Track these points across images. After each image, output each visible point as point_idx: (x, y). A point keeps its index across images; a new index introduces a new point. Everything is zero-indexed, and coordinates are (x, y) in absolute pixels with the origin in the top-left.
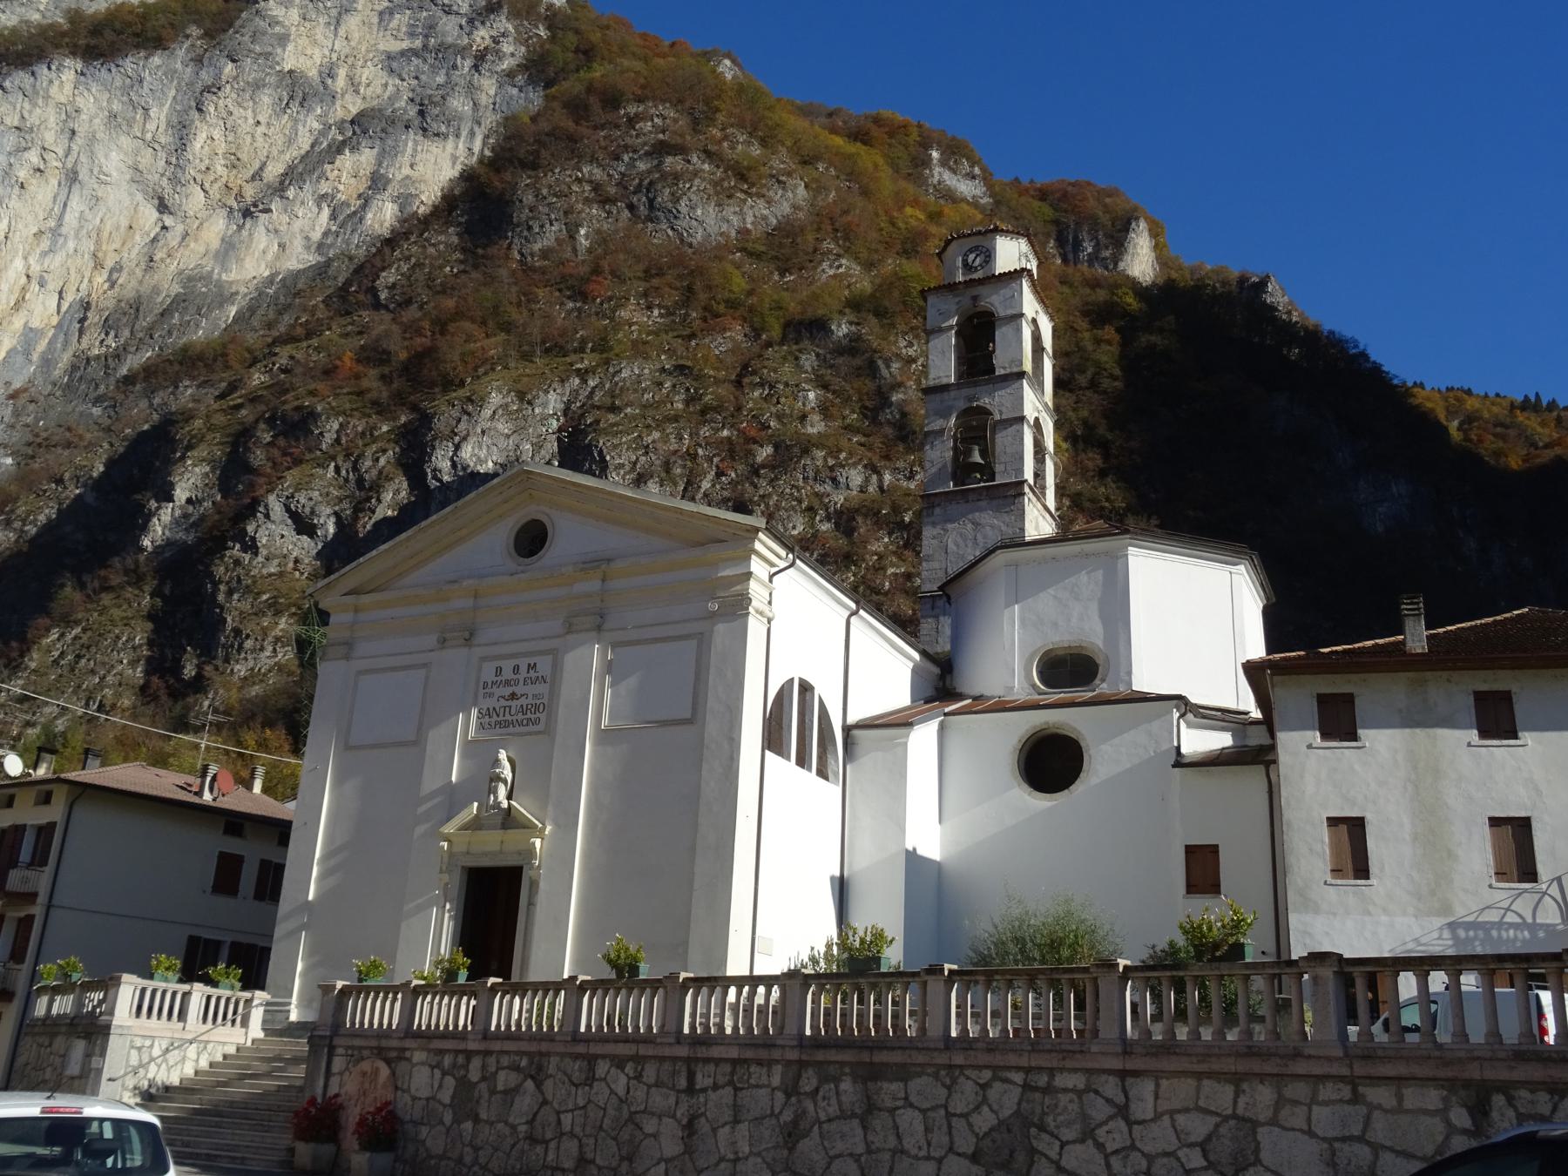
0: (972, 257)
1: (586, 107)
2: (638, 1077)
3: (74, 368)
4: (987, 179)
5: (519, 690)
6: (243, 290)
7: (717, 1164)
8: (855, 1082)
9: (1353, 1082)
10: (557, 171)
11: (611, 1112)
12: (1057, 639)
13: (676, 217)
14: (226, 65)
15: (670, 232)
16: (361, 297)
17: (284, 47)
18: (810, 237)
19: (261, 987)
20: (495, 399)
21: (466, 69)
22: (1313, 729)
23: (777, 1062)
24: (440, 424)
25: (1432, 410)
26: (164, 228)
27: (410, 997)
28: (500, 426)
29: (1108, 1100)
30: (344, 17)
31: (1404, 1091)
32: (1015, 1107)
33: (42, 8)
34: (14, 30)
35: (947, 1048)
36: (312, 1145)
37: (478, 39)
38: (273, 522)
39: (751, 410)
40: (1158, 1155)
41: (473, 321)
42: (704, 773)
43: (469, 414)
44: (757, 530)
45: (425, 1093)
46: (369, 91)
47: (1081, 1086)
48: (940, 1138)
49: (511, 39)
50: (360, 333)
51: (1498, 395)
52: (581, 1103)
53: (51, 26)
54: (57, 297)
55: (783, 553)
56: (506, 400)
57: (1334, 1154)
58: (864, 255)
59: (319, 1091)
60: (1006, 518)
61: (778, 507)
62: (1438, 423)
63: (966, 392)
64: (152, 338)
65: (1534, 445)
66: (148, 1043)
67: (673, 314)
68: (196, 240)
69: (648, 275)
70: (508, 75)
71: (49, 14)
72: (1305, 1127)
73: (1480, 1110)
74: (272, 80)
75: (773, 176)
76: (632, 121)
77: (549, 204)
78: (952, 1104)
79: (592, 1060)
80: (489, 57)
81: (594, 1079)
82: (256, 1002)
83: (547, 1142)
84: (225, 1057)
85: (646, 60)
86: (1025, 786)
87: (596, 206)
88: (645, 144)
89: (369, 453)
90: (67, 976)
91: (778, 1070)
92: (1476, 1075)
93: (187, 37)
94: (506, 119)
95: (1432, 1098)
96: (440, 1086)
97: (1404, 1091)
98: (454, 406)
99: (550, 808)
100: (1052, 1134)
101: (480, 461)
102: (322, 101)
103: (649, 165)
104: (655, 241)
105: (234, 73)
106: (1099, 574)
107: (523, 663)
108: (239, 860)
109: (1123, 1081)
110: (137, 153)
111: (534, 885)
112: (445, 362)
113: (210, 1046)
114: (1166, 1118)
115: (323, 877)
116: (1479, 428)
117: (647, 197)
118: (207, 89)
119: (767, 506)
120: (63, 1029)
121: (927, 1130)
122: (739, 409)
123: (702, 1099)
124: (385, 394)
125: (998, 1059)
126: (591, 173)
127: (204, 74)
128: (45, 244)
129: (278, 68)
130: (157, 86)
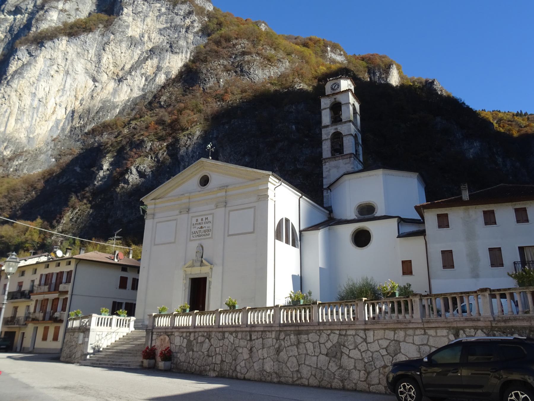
2: (236, 337)
3: (71, 131)
4: (345, 55)
5: (203, 225)
6: (120, 104)
7: (259, 360)
8: (294, 335)
9: (424, 329)
11: (229, 347)
13: (249, 74)
14: (111, 36)
15: (248, 79)
17: (128, 29)
18: (291, 78)
19: (134, 315)
21: (184, 32)
23: (274, 331)
25: (488, 118)
26: (96, 86)
27: (194, 316)
29: (361, 337)
30: (146, 18)
31: (437, 331)
32: (337, 340)
33: (55, 22)
34: (47, 29)
35: (319, 325)
36: (148, 360)
38: (133, 175)
40: (375, 352)
41: (190, 109)
43: (190, 139)
44: (270, 175)
45: (178, 344)
46: (155, 41)
47: (354, 334)
48: (317, 350)
49: (197, 22)
51: (509, 112)
52: (221, 345)
53: (58, 27)
54: (65, 109)
55: (277, 181)
57: (420, 349)
58: (308, 82)
59: (149, 345)
62: (490, 122)
64: (94, 120)
65: (521, 127)
66: (101, 333)
68: (105, 89)
71: (57, 24)
72: (412, 342)
73: (457, 335)
74: (125, 39)
76: (234, 45)
77: (211, 73)
78: (320, 340)
79: (224, 333)
80: (190, 28)
81: (224, 338)
82: (131, 320)
83: (212, 356)
84: (123, 336)
85: (238, 26)
88: (239, 52)
90: (77, 315)
91: (274, 333)
92: (455, 326)
93: (99, 28)
94: (196, 47)
95: (445, 332)
96: (183, 342)
97: (437, 331)
100: (347, 348)
102: (141, 45)
105: (114, 38)
107: (204, 218)
108: (126, 278)
109: (365, 332)
110: (86, 64)
111: (210, 282)
113: (119, 333)
114: (376, 341)
116: (503, 122)
118: (106, 43)
120: (77, 330)
121: (314, 348)
123: (254, 342)
125: (332, 327)
127: (105, 39)
128: (60, 93)
129: (127, 35)
130: (91, 43)
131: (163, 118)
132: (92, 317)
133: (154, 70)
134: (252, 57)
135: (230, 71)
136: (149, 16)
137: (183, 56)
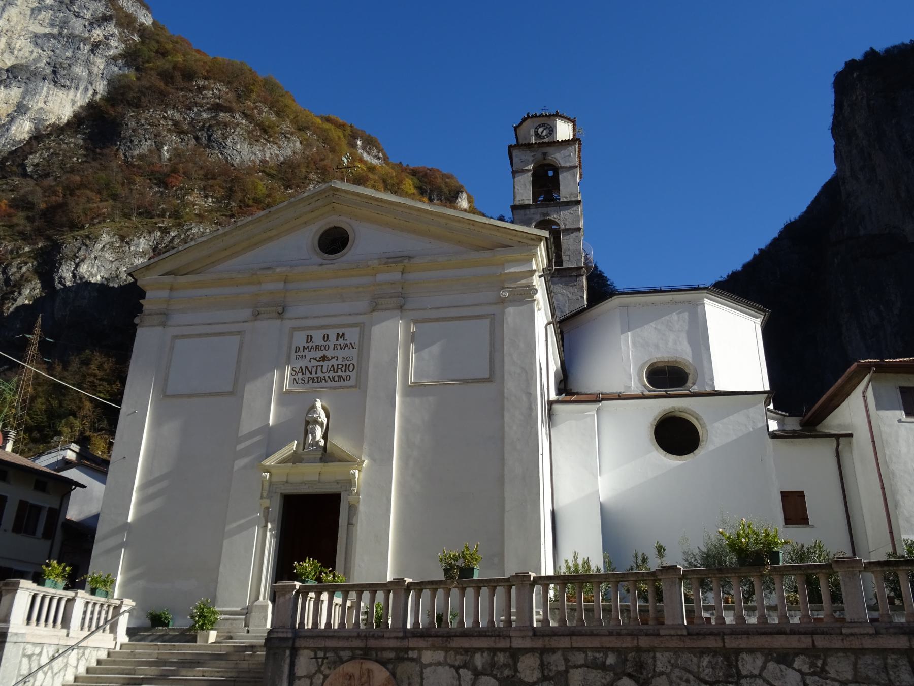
0: (540, 130)
1: (172, 77)
4: (386, 159)
5: (330, 353)
10: (152, 110)
12: (659, 355)
13: (224, 148)
15: (220, 156)
16: (14, 168)
18: (303, 170)
20: (105, 238)
21: (86, 51)
22: (901, 409)
24: (67, 250)
27: (402, 593)
28: (107, 255)
30: (8, 7)
37: (95, 35)
42: (507, 419)
43: (87, 246)
50: (12, 190)
56: (112, 240)
60: (571, 290)
63: (540, 210)
66: (37, 650)
67: (220, 202)
69: (206, 177)
75: (283, 133)
76: (200, 89)
77: (145, 129)
80: (101, 46)
84: (99, 662)
86: (661, 450)
87: (175, 134)
88: (208, 103)
89: (15, 263)
98: (76, 240)
101: (92, 275)
103: (209, 116)
104: (210, 159)
106: (686, 315)
111: (353, 509)
112: (73, 212)
113: (87, 652)
115: (141, 502)
117: (207, 134)
124: (29, 228)
126: (173, 115)
131: (30, 198)
132: (16, 591)
133: (10, 110)
134: (234, 117)
135: (186, 133)
136: (16, 4)
137: (78, 95)
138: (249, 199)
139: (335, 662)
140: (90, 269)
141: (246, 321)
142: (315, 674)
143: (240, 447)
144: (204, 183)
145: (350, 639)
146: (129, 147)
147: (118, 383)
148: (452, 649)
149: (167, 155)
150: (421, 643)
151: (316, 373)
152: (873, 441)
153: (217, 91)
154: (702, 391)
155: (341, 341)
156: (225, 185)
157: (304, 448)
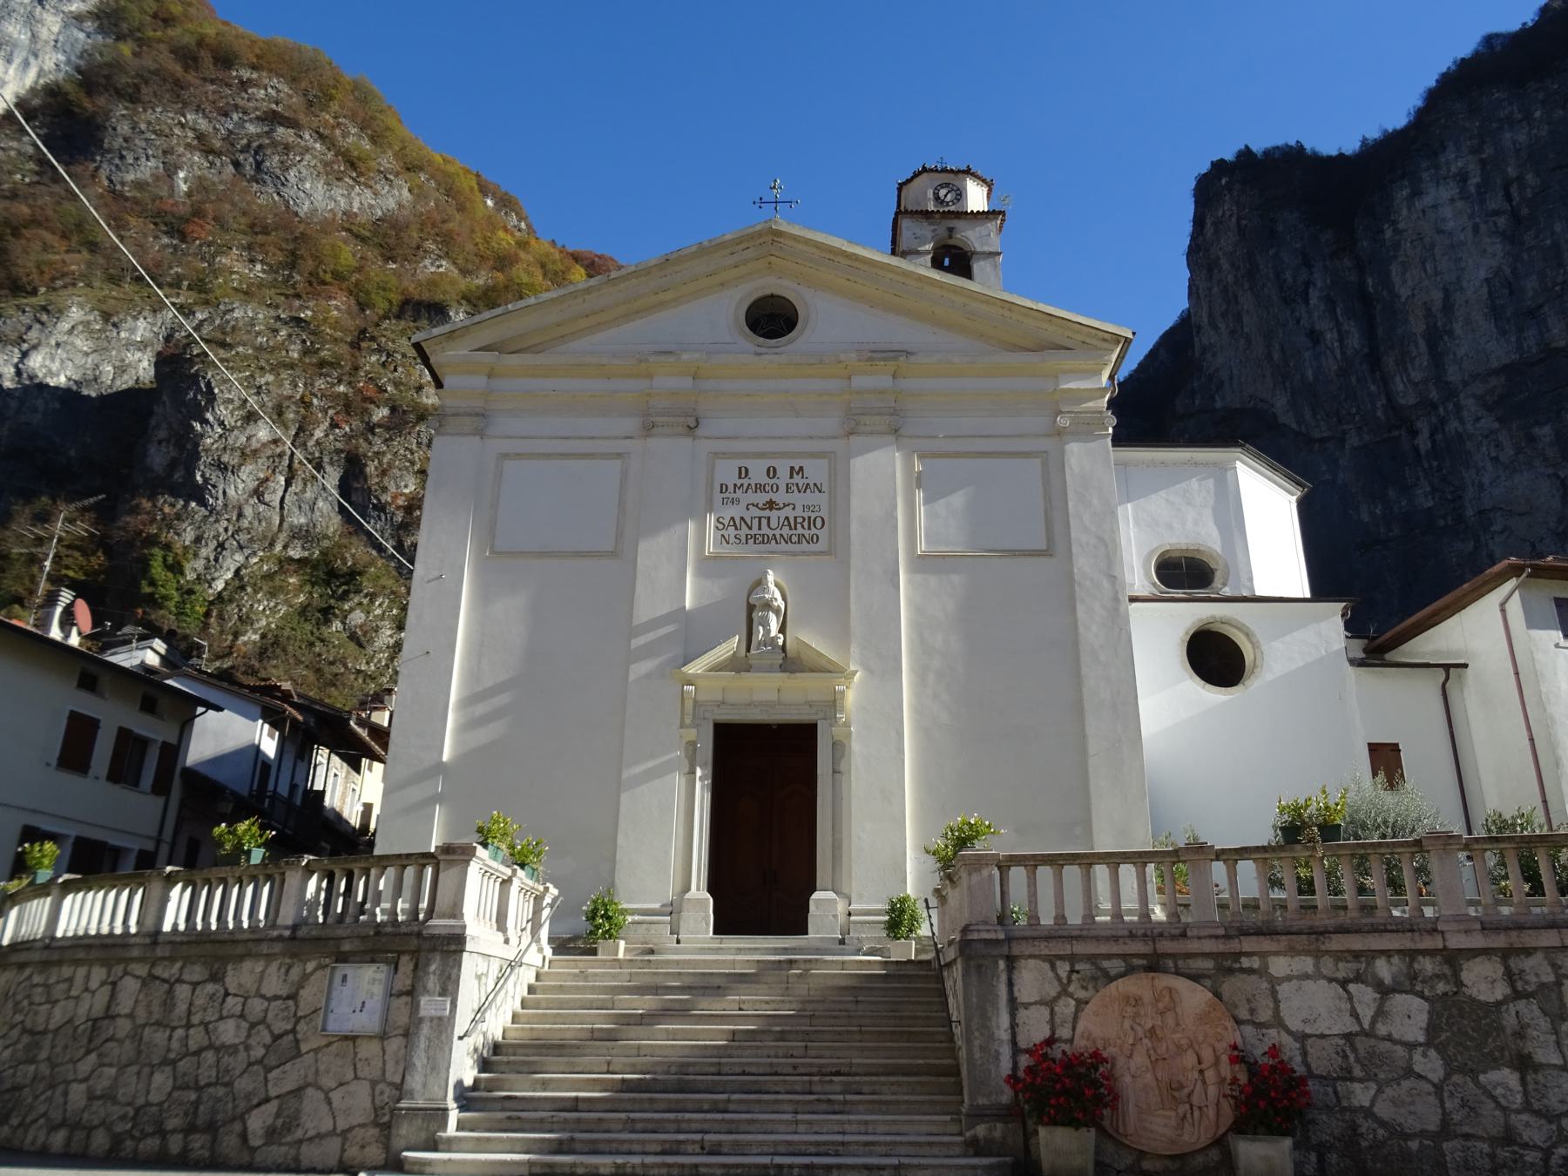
0: (942, 192)
1: (195, 59)
5: (780, 497)
10: (159, 110)
12: (1174, 541)
13: (283, 184)
15: (277, 198)
20: (75, 314)
28: (78, 342)
39: (367, 373)
43: (42, 324)
61: (390, 465)
67: (277, 272)
70: (75, 18)
76: (244, 85)
77: (147, 140)
87: (198, 153)
88: (257, 109)
98: (24, 312)
99: (854, 649)
101: (51, 373)
103: (259, 130)
106: (1210, 483)
111: (839, 748)
112: (17, 265)
115: (464, 728)
119: (380, 463)
122: (356, 368)
126: (195, 122)
132: (467, 862)
134: (301, 137)
135: (218, 154)
137: (11, 71)
138: (325, 272)
139: (1094, 979)
140: (47, 363)
141: (631, 438)
142: (1056, 999)
143: (637, 642)
144: (249, 239)
145: (1121, 940)
146: (117, 166)
147: (100, 554)
148: (1327, 952)
149: (184, 187)
150: (1266, 944)
151: (760, 529)
152: (1517, 674)
153: (271, 91)
154: (1236, 594)
155: (797, 479)
156: (284, 246)
157: (748, 650)
